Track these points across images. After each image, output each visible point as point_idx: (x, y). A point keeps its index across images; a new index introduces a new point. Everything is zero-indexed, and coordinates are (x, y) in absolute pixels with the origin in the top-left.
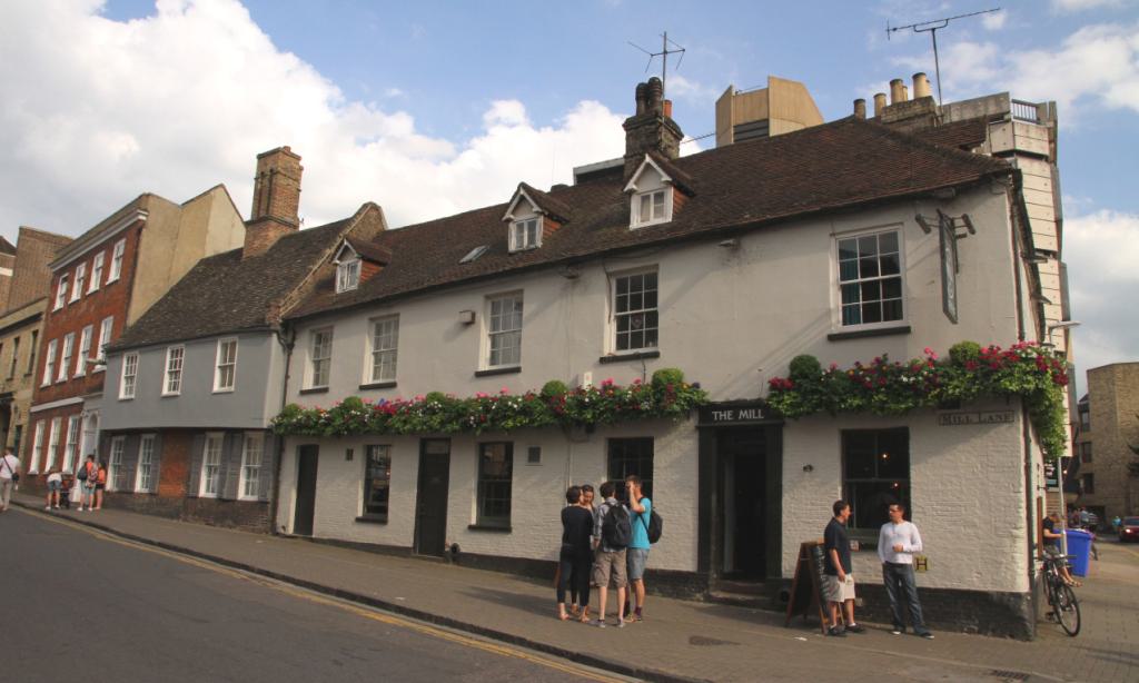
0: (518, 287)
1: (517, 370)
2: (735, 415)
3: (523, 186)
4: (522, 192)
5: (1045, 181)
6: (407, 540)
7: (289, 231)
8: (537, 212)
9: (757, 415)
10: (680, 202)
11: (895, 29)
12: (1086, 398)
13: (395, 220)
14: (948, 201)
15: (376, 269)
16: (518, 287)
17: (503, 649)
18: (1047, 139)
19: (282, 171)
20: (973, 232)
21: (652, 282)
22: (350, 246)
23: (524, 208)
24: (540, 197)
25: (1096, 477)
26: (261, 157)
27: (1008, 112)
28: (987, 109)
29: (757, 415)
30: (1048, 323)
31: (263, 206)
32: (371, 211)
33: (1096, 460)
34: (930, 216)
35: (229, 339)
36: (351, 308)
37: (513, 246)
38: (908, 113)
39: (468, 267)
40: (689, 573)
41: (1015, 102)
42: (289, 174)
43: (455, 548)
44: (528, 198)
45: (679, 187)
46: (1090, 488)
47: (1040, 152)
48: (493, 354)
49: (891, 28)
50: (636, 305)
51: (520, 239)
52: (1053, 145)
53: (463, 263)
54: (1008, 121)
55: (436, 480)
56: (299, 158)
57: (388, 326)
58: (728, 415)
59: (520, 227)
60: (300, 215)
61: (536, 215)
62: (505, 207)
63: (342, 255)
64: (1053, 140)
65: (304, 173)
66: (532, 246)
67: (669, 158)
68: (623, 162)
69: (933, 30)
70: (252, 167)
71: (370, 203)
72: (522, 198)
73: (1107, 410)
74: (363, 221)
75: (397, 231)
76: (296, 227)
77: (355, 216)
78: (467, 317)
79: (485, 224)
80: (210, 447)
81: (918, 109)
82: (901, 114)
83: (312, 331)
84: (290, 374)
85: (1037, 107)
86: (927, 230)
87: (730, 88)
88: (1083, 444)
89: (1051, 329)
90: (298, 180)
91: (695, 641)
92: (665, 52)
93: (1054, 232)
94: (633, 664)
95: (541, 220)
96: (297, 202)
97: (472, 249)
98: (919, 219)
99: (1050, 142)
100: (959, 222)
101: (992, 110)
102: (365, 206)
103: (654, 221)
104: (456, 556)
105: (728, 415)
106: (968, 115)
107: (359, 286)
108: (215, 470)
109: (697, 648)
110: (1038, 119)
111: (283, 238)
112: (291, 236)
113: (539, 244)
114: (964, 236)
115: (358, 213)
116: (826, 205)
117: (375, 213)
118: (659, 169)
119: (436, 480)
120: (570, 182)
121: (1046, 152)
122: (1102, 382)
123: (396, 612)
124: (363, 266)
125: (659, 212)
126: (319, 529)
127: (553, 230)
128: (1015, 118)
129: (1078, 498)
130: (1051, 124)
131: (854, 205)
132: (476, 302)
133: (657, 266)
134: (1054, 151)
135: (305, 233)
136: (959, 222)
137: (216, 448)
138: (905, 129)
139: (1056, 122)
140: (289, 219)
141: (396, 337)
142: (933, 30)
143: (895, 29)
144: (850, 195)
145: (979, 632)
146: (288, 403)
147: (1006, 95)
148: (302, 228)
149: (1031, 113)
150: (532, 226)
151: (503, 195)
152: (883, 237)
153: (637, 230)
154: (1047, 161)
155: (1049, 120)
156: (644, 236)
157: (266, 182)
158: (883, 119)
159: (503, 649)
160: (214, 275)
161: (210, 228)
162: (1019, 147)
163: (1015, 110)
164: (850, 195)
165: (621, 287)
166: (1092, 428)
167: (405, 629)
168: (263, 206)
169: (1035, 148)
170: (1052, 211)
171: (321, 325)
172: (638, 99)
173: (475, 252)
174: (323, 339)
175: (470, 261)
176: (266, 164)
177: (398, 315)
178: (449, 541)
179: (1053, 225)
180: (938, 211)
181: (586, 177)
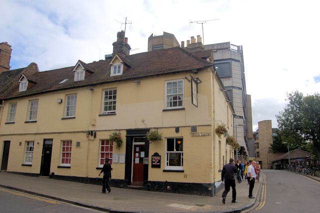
0: (37, 98)
1: (75, 118)
3: (79, 61)
6: (38, 172)
7: (5, 70)
13: (41, 69)
15: (33, 84)
16: (37, 98)
21: (115, 92)
22: (118, 57)
23: (79, 68)
27: (230, 47)
32: (33, 65)
33: (260, 148)
36: (23, 96)
37: (112, 75)
38: (195, 46)
40: (122, 180)
43: (53, 174)
44: (81, 65)
45: (125, 64)
46: (258, 157)
48: (68, 113)
50: (110, 98)
54: (230, 50)
55: (48, 152)
57: (72, 98)
59: (115, 67)
60: (10, 65)
62: (74, 67)
63: (114, 61)
65: (12, 51)
68: (112, 56)
72: (79, 64)
78: (60, 101)
79: (68, 72)
81: (198, 45)
83: (10, 104)
90: (10, 54)
101: (225, 46)
103: (117, 74)
104: (53, 176)
106: (210, 48)
112: (6, 72)
113: (83, 79)
118: (119, 58)
119: (48, 152)
120: (104, 59)
125: (119, 71)
126: (9, 169)
131: (169, 73)
132: (62, 96)
135: (11, 71)
140: (7, 67)
141: (76, 101)
144: (171, 70)
147: (229, 43)
148: (11, 69)
149: (236, 48)
150: (119, 67)
151: (73, 63)
152: (114, 91)
153: (112, 77)
156: (114, 78)
163: (232, 47)
164: (171, 70)
165: (106, 94)
171: (34, 98)
173: (65, 80)
174: (14, 106)
177: (38, 99)
178: (51, 171)
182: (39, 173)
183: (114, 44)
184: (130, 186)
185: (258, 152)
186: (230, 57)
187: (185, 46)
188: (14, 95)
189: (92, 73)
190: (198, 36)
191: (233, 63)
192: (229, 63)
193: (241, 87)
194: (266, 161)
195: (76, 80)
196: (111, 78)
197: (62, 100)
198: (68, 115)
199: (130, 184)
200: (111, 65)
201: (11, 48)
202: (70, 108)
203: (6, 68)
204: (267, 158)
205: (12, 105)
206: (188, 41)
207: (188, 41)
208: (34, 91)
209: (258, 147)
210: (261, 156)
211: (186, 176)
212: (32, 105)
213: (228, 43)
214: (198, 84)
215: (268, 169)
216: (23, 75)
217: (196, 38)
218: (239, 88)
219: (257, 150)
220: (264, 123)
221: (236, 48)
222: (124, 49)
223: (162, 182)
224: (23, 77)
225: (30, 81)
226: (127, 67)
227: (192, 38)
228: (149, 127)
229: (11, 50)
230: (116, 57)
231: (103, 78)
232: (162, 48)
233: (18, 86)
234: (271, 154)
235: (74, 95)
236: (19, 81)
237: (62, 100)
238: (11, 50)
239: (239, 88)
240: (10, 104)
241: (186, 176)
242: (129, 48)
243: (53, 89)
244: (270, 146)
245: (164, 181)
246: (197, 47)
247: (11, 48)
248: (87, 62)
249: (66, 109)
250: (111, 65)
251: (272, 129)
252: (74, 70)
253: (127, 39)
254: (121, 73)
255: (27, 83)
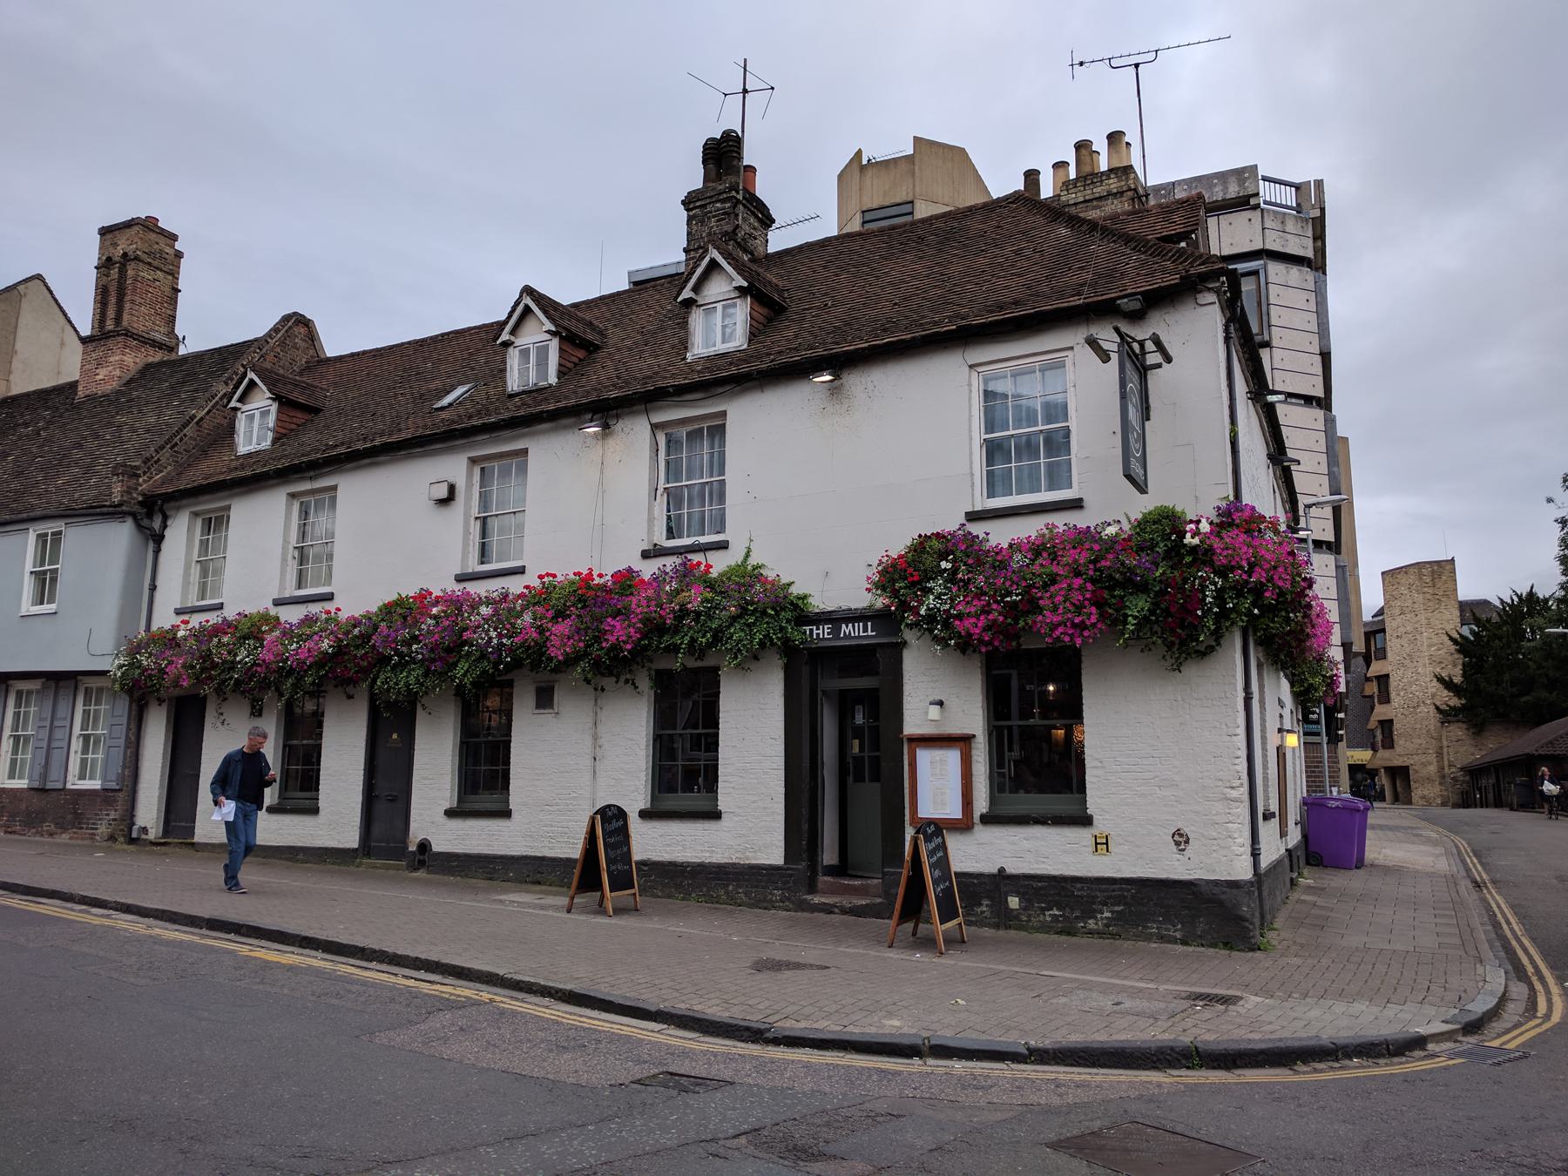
2: (836, 631)
3: (528, 291)
4: (528, 301)
5: (1305, 295)
6: (770, 850)
7: (157, 356)
8: (548, 332)
9: (865, 630)
10: (761, 319)
11: (1081, 64)
12: (1381, 612)
13: (335, 344)
14: (1137, 317)
15: (300, 417)
17: (458, 991)
18: (1310, 234)
19: (144, 257)
20: (1168, 359)
24: (556, 310)
25: (1396, 725)
26: (105, 232)
28: (1225, 189)
29: (865, 630)
30: (1302, 501)
31: (111, 313)
34: (1108, 337)
35: (50, 527)
37: (514, 383)
38: (1100, 190)
39: (444, 415)
41: (1265, 179)
42: (156, 263)
43: (424, 846)
47: (1301, 253)
48: (483, 547)
49: (1076, 61)
51: (524, 372)
52: (1319, 243)
53: (442, 409)
54: (1257, 206)
56: (174, 238)
57: (505, 474)
58: (824, 631)
59: (525, 353)
60: (179, 331)
61: (548, 336)
62: (501, 325)
64: (1319, 237)
66: (543, 384)
67: (752, 253)
69: (1137, 66)
70: (91, 253)
71: (295, 313)
72: (527, 310)
73: (1409, 628)
74: (282, 343)
75: (340, 359)
76: (172, 349)
77: (269, 335)
78: (443, 492)
80: (18, 705)
81: (1113, 184)
82: (1089, 192)
84: (158, 583)
85: (1298, 187)
86: (1104, 356)
87: (859, 153)
88: (1378, 678)
89: (1308, 506)
90: (174, 274)
91: (762, 966)
92: (745, 91)
93: (1318, 369)
94: (652, 1002)
95: (554, 344)
96: (175, 309)
97: (453, 388)
98: (1092, 343)
99: (1315, 239)
100: (1150, 346)
101: (1233, 191)
102: (286, 318)
104: (424, 856)
105: (824, 631)
107: (275, 441)
108: (97, 742)
109: (765, 976)
110: (1298, 205)
111: (148, 366)
112: (162, 364)
113: (553, 379)
114: (1159, 366)
115: (275, 329)
116: (964, 322)
117: (303, 330)
121: (1309, 253)
122: (1403, 590)
123: (301, 946)
124: (279, 411)
127: (575, 359)
128: (1265, 202)
129: (1373, 756)
130: (1317, 213)
132: (453, 467)
133: (724, 414)
134: (1321, 251)
135: (185, 359)
136: (1150, 346)
137: (98, 703)
138: (1093, 214)
139: (1323, 210)
142: (1137, 66)
143: (1081, 64)
145: (1184, 943)
146: (154, 628)
148: (182, 351)
149: (1288, 197)
150: (543, 352)
154: (1309, 266)
155: (1313, 207)
157: (114, 273)
158: (1063, 199)
159: (458, 991)
160: (26, 425)
161: (18, 346)
162: (1271, 246)
163: (1267, 192)
166: (1389, 654)
167: (191, 946)
168: (111, 313)
169: (1294, 247)
170: (1316, 339)
171: (210, 505)
172: (704, 162)
174: (215, 523)
175: (450, 405)
176: (115, 245)
177: (335, 488)
179: (1318, 359)
180: (1117, 330)
181: (642, 285)
182: (356, 845)
183: (688, 203)
184: (817, 899)
185: (1387, 725)
186: (1257, 246)
187: (1047, 190)
188: (212, 468)
189: (591, 348)
190: (1114, 138)
191: (1275, 270)
192: (1255, 273)
193: (1320, 393)
194: (1433, 768)
195: (514, 383)
196: (238, 458)
197: (452, 489)
198: (484, 556)
199: (812, 889)
200: (506, 344)
201: (178, 246)
202: (494, 524)
203: (160, 346)
204: (1440, 754)
205: (208, 524)
206: (1060, 166)
207: (1060, 166)
208: (313, 441)
209: (1385, 698)
210: (1400, 743)
211: (1102, 844)
212: (305, 514)
213: (1246, 174)
214: (1153, 377)
215: (1443, 804)
216: (251, 375)
217: (1100, 145)
218: (1308, 400)
219: (1381, 712)
220: (1412, 578)
221: (1288, 197)
222: (746, 222)
223: (980, 876)
224: (252, 384)
225: (283, 401)
226: (764, 311)
227: (1082, 147)
228: (1529, 590)
229: (179, 255)
230: (252, 381)
231: (646, 367)
232: (909, 218)
233: (231, 430)
234: (1457, 731)
235: (327, 496)
236: (233, 404)
237: (452, 489)
238: (179, 255)
239: (1308, 400)
240: (196, 514)
241: (1102, 844)
242: (767, 221)
243: (405, 435)
244: (1447, 698)
245: (990, 868)
246: (1110, 194)
247: (178, 246)
248: (565, 296)
249: (476, 528)
250: (506, 344)
251: (1460, 602)
252: (505, 337)
253: (751, 169)
254: (266, 444)
255: (271, 420)
